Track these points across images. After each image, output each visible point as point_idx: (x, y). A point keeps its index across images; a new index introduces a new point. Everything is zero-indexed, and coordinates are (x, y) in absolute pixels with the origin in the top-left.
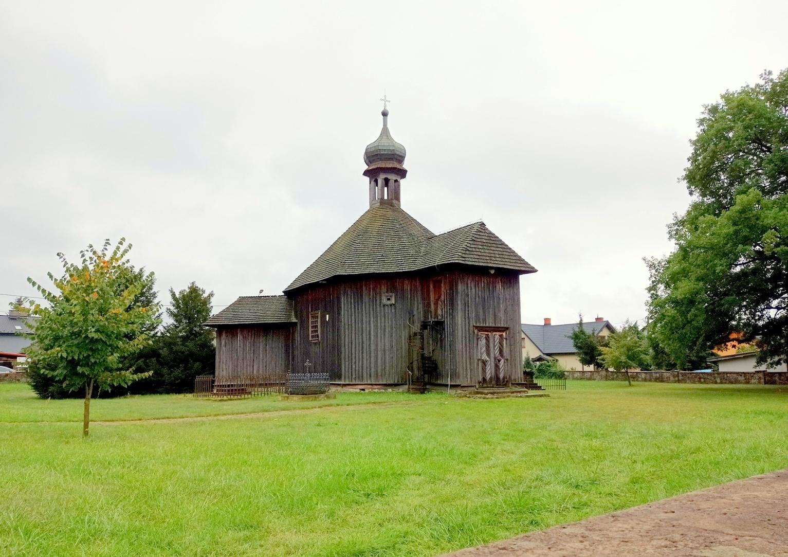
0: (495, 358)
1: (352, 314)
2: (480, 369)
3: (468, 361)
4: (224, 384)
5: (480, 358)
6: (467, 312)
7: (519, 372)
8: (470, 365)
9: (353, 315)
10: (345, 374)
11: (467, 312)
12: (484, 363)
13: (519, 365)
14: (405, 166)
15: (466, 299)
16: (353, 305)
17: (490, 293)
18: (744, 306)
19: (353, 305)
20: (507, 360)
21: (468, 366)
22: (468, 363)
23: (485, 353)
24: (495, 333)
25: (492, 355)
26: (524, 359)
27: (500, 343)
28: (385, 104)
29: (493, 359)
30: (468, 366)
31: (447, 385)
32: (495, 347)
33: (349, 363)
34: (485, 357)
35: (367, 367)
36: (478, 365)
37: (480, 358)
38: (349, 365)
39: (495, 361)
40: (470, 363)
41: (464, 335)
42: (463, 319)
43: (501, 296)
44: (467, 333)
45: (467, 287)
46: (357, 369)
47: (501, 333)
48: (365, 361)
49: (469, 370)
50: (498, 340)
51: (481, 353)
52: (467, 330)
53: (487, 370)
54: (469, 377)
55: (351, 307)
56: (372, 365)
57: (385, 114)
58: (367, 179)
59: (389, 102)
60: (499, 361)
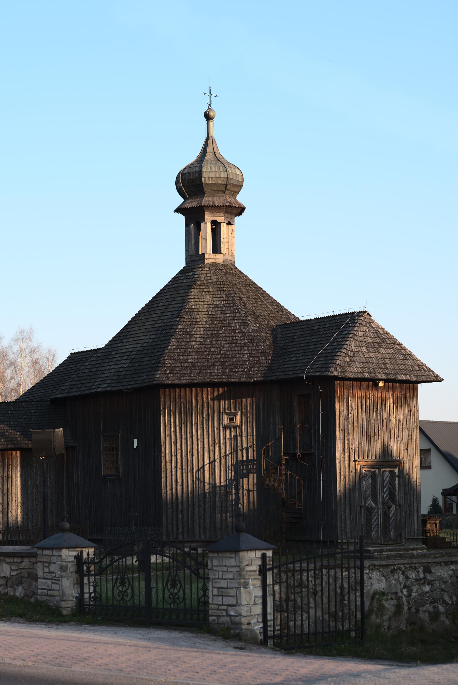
0: (383, 504)
1: (176, 440)
2: (363, 519)
3: (348, 509)
4: (9, 539)
5: (363, 504)
6: (346, 442)
7: (416, 523)
8: (350, 514)
9: (178, 441)
10: (167, 526)
11: (346, 442)
12: (369, 510)
13: (416, 514)
14: (241, 198)
15: (346, 423)
16: (178, 428)
17: (377, 414)
18: (183, 551)
19: (178, 428)
20: (400, 505)
21: (348, 516)
22: (348, 511)
23: (370, 497)
24: (383, 469)
25: (380, 500)
26: (259, 640)
27: (390, 483)
28: (210, 101)
29: (380, 505)
30: (348, 516)
31: (318, 542)
32: (384, 488)
33: (173, 511)
34: (370, 502)
35: (199, 517)
36: (361, 514)
37: (363, 504)
38: (172, 514)
39: (383, 508)
40: (350, 511)
41: (342, 473)
42: (342, 452)
43: (392, 418)
44: (347, 470)
45: (347, 406)
46: (185, 519)
47: (392, 469)
48: (197, 509)
49: (348, 522)
50: (388, 479)
51: (364, 498)
52: (347, 466)
53: (373, 521)
54: (348, 530)
55: (175, 431)
56: (208, 515)
57: (208, 117)
58: (181, 218)
59: (216, 96)
60: (389, 508)
